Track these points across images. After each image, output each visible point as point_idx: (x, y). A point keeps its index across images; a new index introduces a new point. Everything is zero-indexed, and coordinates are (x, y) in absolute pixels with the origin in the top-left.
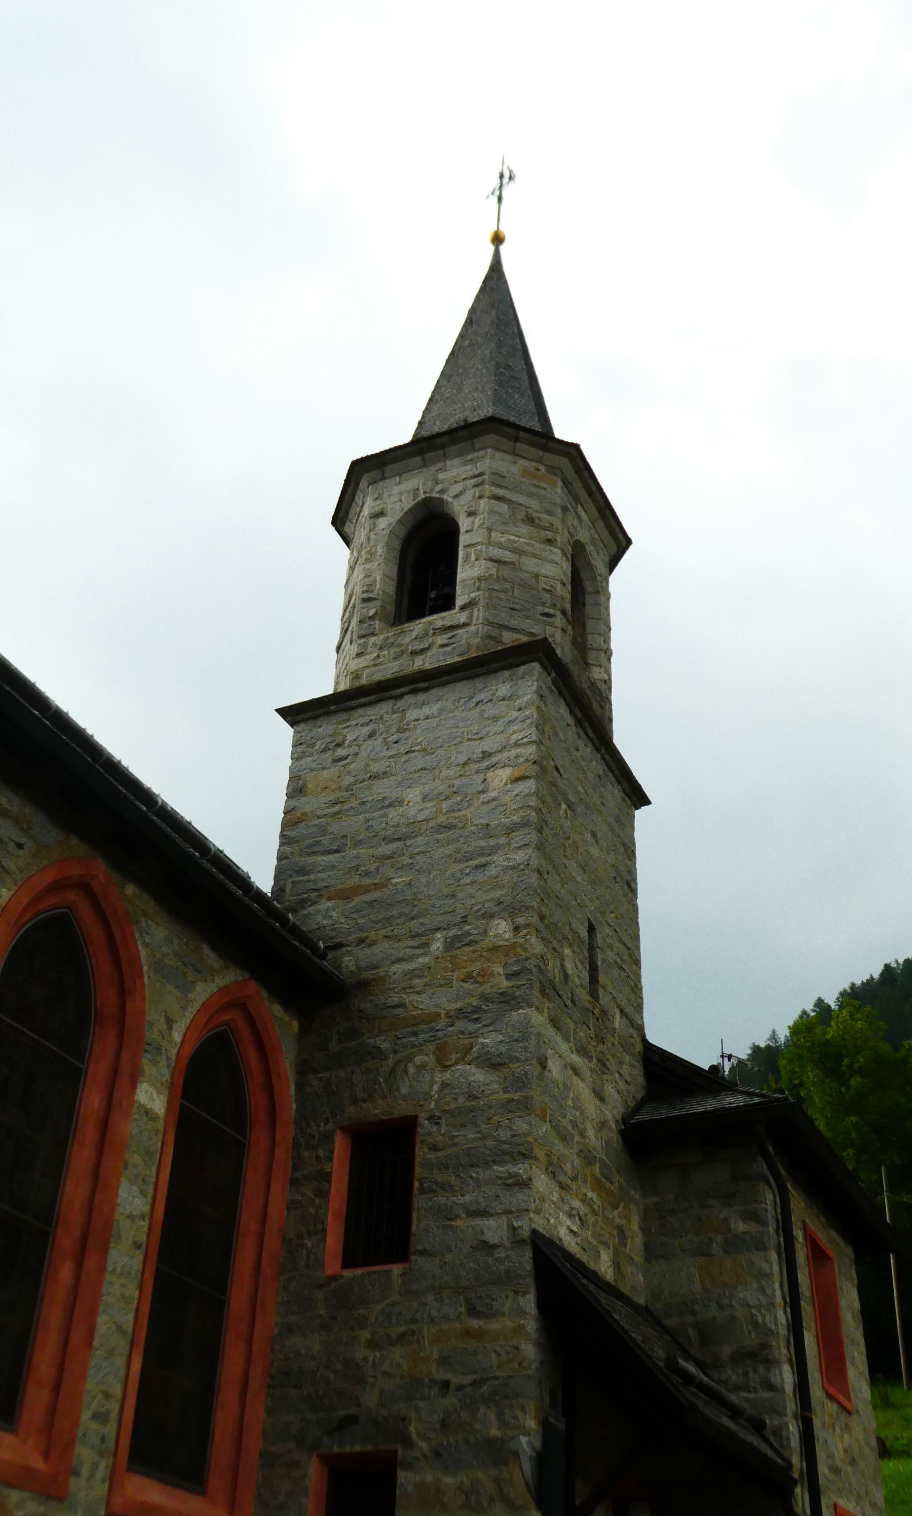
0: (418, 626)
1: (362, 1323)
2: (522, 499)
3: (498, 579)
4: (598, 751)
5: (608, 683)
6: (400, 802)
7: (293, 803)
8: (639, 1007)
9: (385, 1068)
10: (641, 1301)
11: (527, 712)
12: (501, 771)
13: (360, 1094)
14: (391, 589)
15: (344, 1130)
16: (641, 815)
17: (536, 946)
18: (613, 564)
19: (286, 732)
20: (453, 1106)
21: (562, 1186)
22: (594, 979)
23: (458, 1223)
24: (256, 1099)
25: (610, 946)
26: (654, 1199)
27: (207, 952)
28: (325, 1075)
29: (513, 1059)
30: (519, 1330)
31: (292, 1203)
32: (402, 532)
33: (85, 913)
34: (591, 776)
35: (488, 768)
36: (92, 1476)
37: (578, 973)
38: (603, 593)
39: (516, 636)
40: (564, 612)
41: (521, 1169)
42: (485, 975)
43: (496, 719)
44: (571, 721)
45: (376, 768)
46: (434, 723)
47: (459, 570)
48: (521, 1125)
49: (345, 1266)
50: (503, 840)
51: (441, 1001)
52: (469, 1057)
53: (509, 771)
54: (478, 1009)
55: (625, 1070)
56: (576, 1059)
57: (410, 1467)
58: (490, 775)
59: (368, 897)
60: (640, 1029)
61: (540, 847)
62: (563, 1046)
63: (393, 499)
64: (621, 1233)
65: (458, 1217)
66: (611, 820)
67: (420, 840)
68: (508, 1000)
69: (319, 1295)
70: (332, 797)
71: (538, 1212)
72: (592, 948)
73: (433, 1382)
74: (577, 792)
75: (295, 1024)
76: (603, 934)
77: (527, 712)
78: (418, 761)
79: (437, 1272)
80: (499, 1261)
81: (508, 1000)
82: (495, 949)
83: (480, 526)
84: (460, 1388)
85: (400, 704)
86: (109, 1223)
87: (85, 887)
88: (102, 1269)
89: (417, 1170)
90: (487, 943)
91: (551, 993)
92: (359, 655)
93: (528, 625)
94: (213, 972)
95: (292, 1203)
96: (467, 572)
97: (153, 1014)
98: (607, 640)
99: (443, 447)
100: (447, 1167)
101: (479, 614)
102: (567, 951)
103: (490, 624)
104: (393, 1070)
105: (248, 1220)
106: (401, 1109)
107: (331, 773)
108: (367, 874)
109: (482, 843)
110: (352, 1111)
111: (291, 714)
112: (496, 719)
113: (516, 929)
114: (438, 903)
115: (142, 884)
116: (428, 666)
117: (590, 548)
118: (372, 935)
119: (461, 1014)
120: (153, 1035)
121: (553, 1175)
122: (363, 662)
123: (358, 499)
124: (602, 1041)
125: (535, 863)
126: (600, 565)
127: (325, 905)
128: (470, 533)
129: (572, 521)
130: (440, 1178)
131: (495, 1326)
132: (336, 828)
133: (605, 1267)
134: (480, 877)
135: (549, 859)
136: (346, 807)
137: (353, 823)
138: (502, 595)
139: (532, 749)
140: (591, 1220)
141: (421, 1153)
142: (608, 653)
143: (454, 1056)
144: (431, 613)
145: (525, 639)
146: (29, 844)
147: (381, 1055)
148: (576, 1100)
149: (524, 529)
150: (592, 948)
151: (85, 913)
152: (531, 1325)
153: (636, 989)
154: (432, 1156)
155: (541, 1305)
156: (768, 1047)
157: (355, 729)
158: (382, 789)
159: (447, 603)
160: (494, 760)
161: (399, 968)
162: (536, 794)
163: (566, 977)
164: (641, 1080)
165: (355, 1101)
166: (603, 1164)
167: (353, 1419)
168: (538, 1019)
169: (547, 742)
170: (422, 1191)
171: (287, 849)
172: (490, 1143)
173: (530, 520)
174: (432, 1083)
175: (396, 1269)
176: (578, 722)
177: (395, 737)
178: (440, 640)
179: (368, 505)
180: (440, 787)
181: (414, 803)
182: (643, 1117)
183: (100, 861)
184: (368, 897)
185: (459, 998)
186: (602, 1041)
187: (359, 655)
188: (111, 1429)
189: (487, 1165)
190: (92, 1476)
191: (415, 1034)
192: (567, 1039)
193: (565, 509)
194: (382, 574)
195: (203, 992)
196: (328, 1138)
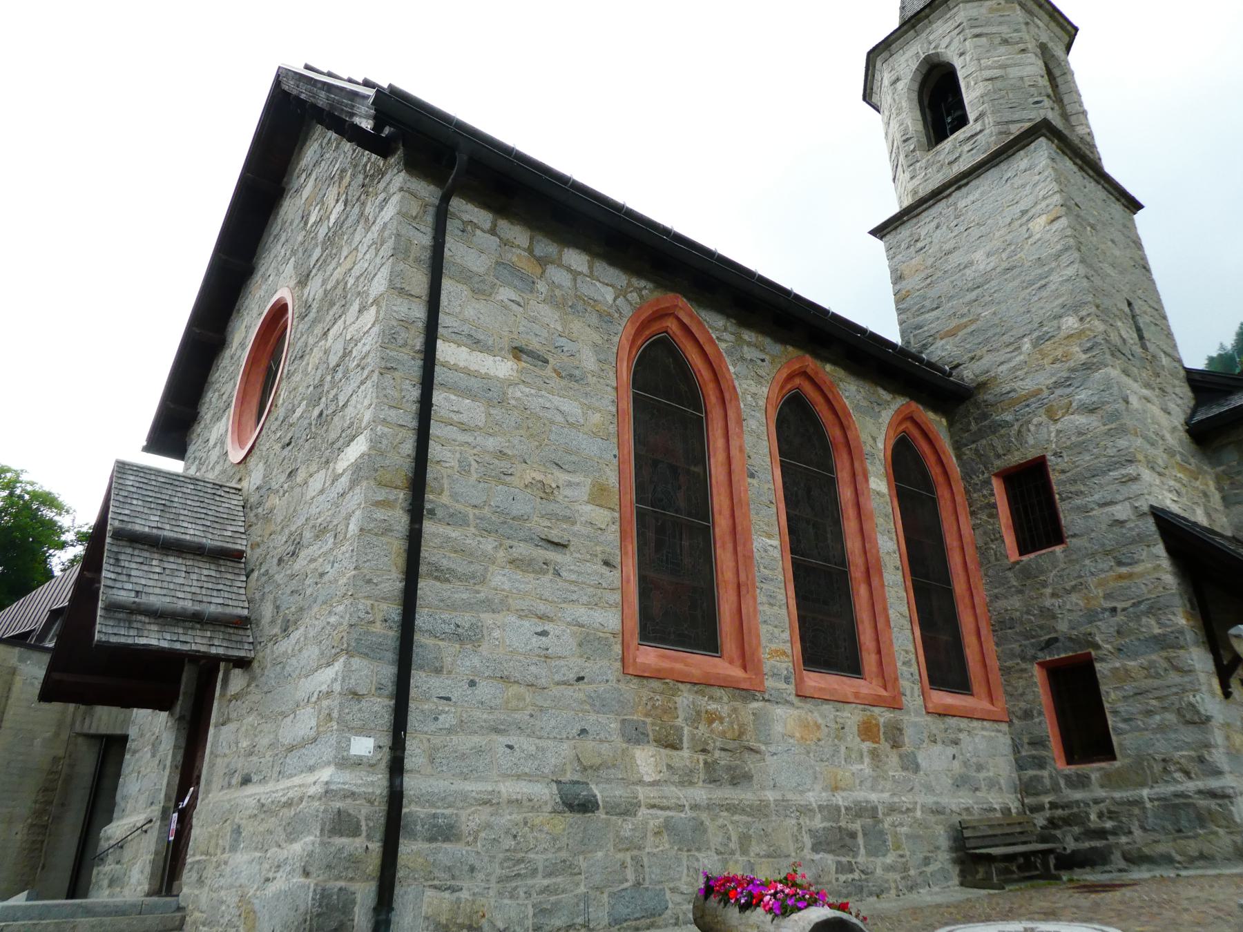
0: (947, 144)
1: (1044, 584)
2: (994, 30)
3: (995, 92)
4: (1098, 183)
5: (1090, 134)
6: (972, 263)
7: (898, 287)
8: (1175, 346)
9: (1013, 432)
10: (1229, 534)
11: (1046, 173)
12: (1038, 220)
13: (1001, 452)
14: (920, 126)
15: (996, 475)
16: (1139, 217)
17: (1099, 326)
18: (1068, 48)
19: (878, 245)
20: (1068, 443)
21: (1160, 474)
22: (1141, 337)
23: (1094, 512)
24: (935, 471)
25: (1145, 312)
26: (1222, 468)
27: (881, 392)
28: (974, 446)
29: (1103, 403)
30: (1157, 568)
31: (978, 528)
32: (916, 86)
33: (808, 389)
34: (1099, 203)
35: (1028, 220)
36: (912, 695)
37: (1130, 335)
38: (1067, 72)
39: (1019, 125)
40: (1048, 96)
41: (1131, 470)
42: (1067, 356)
43: (1023, 186)
44: (1075, 168)
45: (947, 247)
46: (979, 204)
47: (964, 96)
48: (1122, 443)
49: (1021, 554)
50: (1054, 265)
51: (1042, 380)
52: (1071, 410)
53: (1044, 217)
54: (1068, 378)
55: (1178, 390)
56: (1146, 392)
57: (1102, 660)
58: (1031, 225)
59: (969, 329)
60: (1180, 361)
61: (1083, 261)
62: (1135, 386)
63: (902, 66)
64: (1205, 495)
65: (1092, 509)
66: (1120, 227)
67: (993, 283)
68: (1088, 367)
69: (1009, 574)
70: (923, 275)
71: (1149, 494)
72: (1133, 317)
73: (1105, 610)
74: (1094, 216)
75: (944, 420)
76: (1138, 305)
77: (1046, 173)
78: (975, 232)
79: (1087, 545)
80: (1131, 529)
81: (1088, 367)
82: (1070, 336)
83: (971, 60)
84: (1124, 610)
85: (951, 200)
86: (878, 560)
87: (804, 374)
88: (883, 586)
89: (1055, 487)
90: (1062, 334)
91: (1118, 354)
92: (912, 178)
93: (1025, 115)
94: (888, 403)
95: (978, 528)
96: (971, 95)
97: (864, 436)
98: (1081, 104)
99: (927, 16)
100: (1075, 481)
101: (989, 120)
102: (1119, 324)
103: (999, 123)
104: (1019, 431)
105: (951, 541)
106: (1032, 454)
107: (918, 259)
108: (963, 316)
109: (1040, 271)
110: (999, 464)
111: (880, 232)
112: (1023, 186)
113: (1081, 319)
114: (1019, 319)
115: (834, 363)
116: (963, 169)
117: (1050, 45)
118: (979, 353)
119: (1057, 385)
120: (867, 449)
121: (1153, 468)
122: (916, 182)
123: (878, 76)
124: (1158, 375)
125: (1082, 271)
126: (1058, 51)
127: (939, 343)
128: (965, 71)
129: (1034, 30)
130: (1073, 489)
131: (1138, 569)
132: (933, 293)
133: (1200, 517)
134: (1044, 293)
135: (1090, 266)
136: (934, 278)
137: (943, 287)
138: (1001, 101)
139: (1057, 197)
140: (1183, 490)
141: (1054, 477)
142: (1084, 113)
143: (1060, 413)
144: (952, 132)
145: (1027, 125)
146: (767, 358)
147: (1008, 425)
148: (1153, 417)
149: (1003, 49)
150: (1133, 317)
151: (808, 389)
152: (1166, 563)
153: (1169, 335)
154: (1063, 477)
155: (1169, 550)
156: (1220, 355)
157: (925, 226)
158: (955, 259)
159: (962, 121)
160: (1030, 214)
161: (1004, 368)
162: (1069, 226)
163: (1124, 340)
164: (1190, 394)
165: (999, 456)
166: (1181, 454)
167: (1056, 640)
168: (1115, 373)
169: (1065, 189)
170: (1062, 500)
171: (904, 317)
172: (1104, 460)
173: (1005, 42)
174: (1049, 433)
175: (1058, 549)
176: (1081, 168)
177: (955, 223)
178: (966, 148)
179: (885, 76)
180: (997, 243)
181: (981, 260)
182: (1199, 417)
183: (807, 356)
184: (969, 329)
185: (1053, 375)
186: (1158, 375)
187: (912, 178)
188: (914, 669)
189: (1104, 473)
190: (912, 695)
191: (1028, 406)
192: (1136, 381)
193: (1027, 24)
194: (912, 120)
195: (887, 415)
196: (987, 483)
